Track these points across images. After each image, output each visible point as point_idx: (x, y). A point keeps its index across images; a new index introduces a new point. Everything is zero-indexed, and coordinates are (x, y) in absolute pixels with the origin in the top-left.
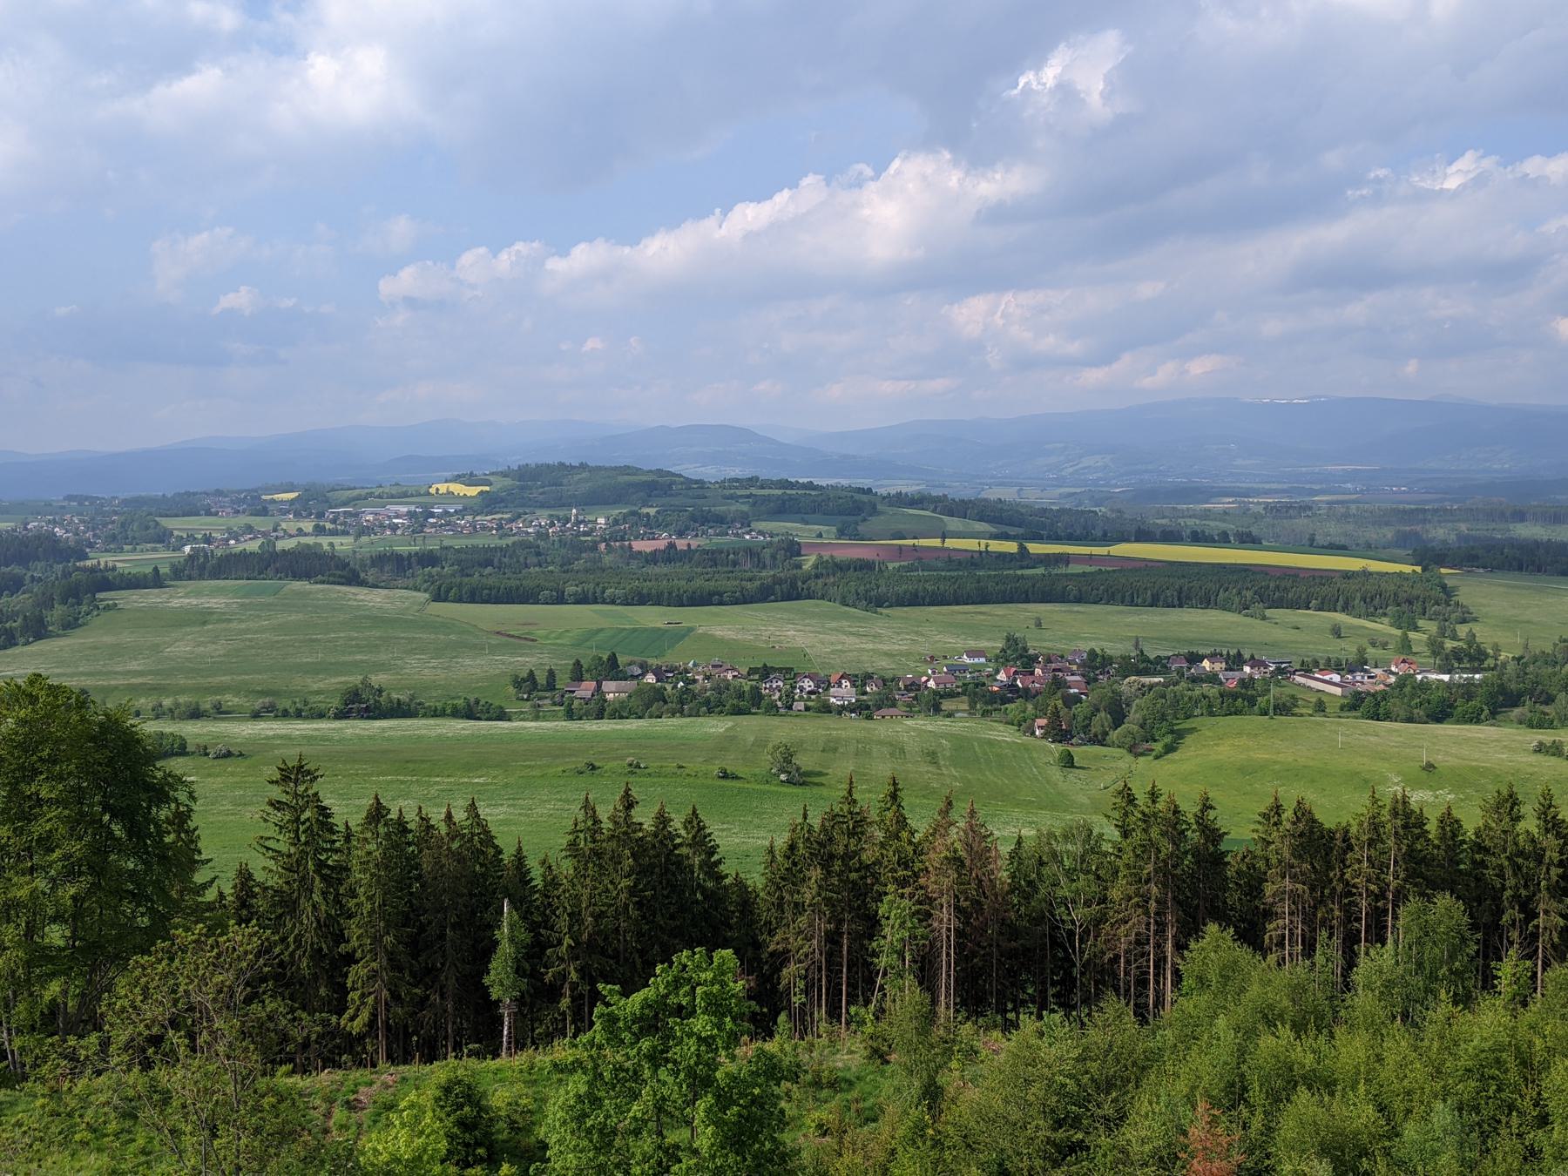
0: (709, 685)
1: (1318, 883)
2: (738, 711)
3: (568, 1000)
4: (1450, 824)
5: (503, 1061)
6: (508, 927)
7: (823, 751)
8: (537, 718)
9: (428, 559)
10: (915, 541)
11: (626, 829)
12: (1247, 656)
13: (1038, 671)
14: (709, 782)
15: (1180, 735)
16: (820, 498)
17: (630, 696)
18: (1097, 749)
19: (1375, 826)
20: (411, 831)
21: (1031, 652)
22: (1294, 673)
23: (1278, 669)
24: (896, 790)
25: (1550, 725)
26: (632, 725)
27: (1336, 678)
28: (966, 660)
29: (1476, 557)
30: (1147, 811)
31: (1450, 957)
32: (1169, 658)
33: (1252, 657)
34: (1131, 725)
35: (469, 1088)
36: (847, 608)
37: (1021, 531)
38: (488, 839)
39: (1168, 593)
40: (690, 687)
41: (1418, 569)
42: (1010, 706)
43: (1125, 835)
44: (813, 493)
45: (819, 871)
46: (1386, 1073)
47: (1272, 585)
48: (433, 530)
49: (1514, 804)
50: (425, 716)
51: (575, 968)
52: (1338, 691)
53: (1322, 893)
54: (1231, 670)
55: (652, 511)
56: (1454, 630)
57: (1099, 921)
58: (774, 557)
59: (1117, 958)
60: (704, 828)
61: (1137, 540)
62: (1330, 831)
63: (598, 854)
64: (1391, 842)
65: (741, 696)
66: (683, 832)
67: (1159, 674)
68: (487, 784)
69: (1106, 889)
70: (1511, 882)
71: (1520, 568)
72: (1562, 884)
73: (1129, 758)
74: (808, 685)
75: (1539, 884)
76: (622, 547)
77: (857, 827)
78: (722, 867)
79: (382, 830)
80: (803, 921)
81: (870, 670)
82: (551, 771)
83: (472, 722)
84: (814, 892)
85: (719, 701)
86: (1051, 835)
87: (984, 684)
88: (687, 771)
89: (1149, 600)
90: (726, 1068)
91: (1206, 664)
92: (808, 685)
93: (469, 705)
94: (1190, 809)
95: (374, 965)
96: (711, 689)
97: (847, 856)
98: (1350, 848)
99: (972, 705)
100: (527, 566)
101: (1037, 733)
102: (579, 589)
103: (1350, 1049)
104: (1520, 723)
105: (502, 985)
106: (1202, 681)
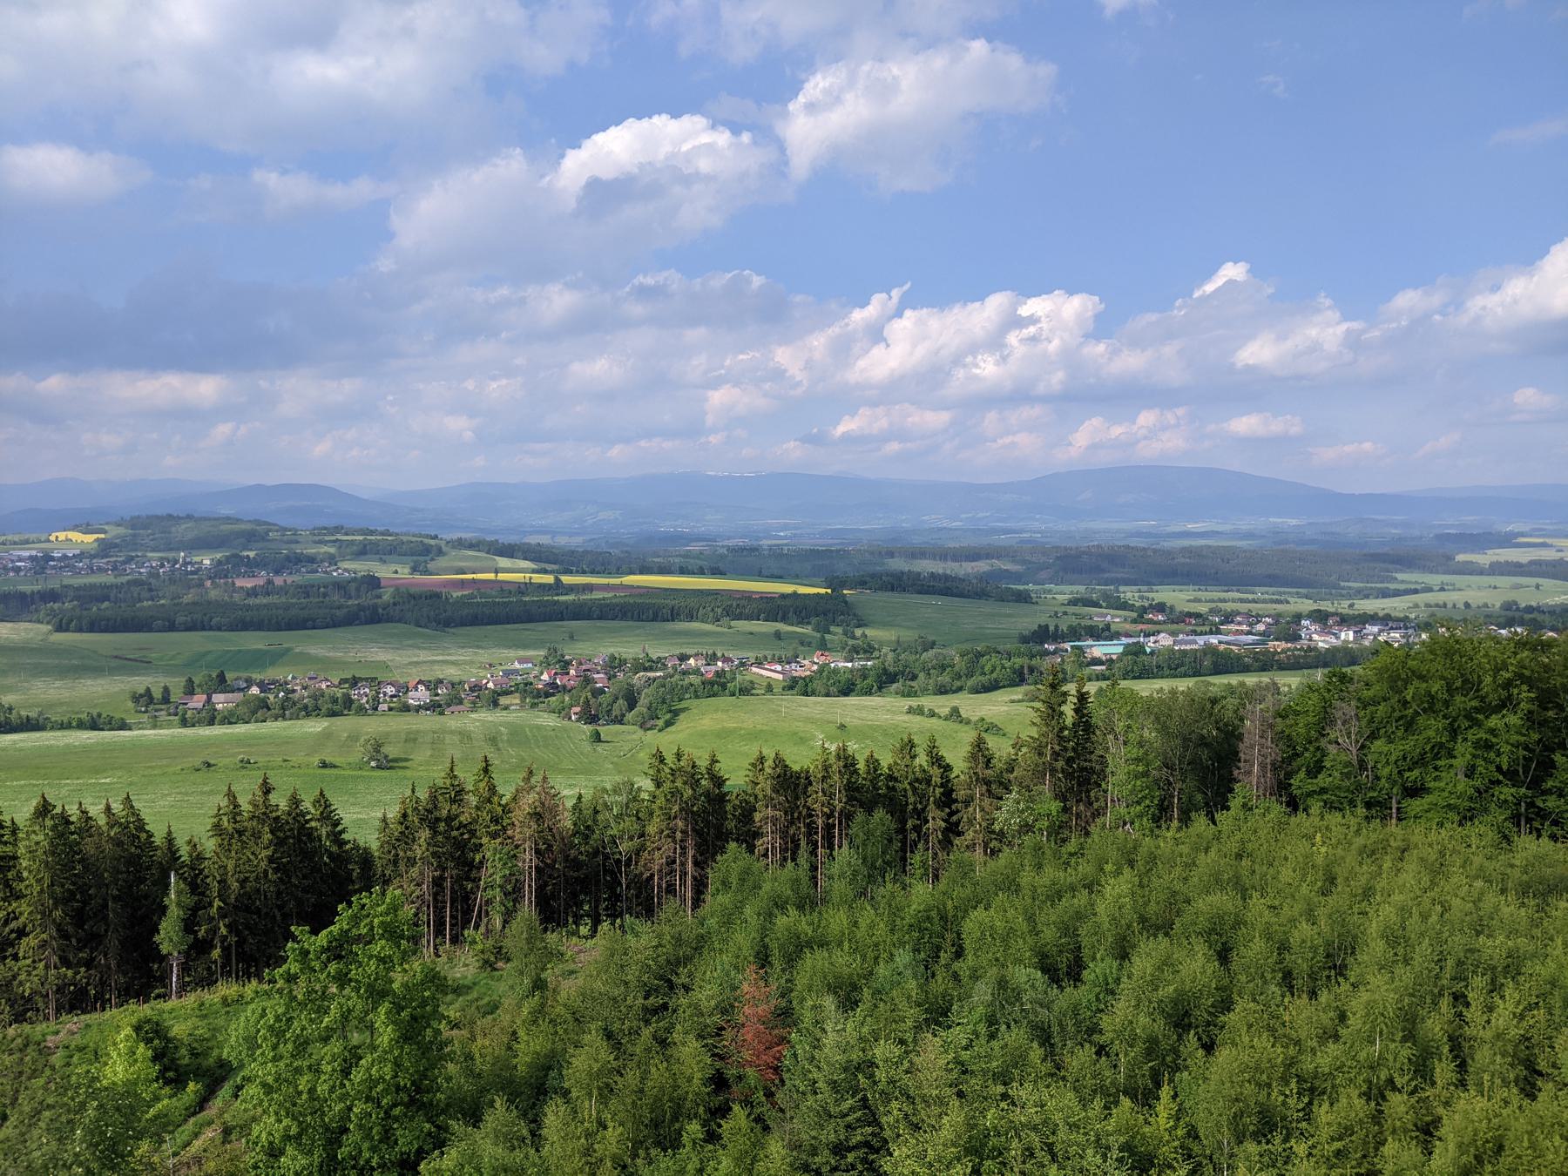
0: (306, 694)
1: (791, 811)
2: (333, 714)
3: (219, 950)
4: (873, 763)
5: (173, 1003)
6: (175, 894)
7: (406, 741)
8: (154, 727)
9: (52, 596)
10: (474, 576)
11: (265, 814)
12: (719, 655)
13: (572, 672)
14: (311, 771)
15: (676, 713)
16: (395, 543)
17: (237, 705)
18: (618, 727)
19: (826, 768)
20: (73, 823)
21: (567, 657)
22: (751, 665)
23: (741, 663)
24: (487, 765)
25: (916, 695)
26: (240, 729)
27: (779, 668)
28: (517, 665)
29: (865, 583)
30: (673, 767)
31: (883, 853)
32: (666, 658)
33: (723, 655)
34: (641, 708)
35: (157, 1025)
36: (420, 629)
37: (555, 567)
38: (141, 825)
39: (664, 611)
40: (290, 696)
41: (829, 591)
42: (552, 699)
43: (658, 785)
44: (390, 538)
45: (428, 832)
46: (861, 933)
47: (735, 604)
48: (54, 571)
49: (912, 747)
50: (52, 729)
51: (224, 925)
52: (780, 677)
53: (792, 816)
54: (709, 665)
55: (252, 554)
56: (853, 632)
57: (642, 848)
58: (358, 590)
59: (652, 875)
60: (330, 805)
61: (641, 573)
62: (796, 772)
63: (240, 833)
64: (836, 777)
65: (335, 701)
66: (313, 811)
67: (660, 669)
68: (114, 783)
69: (644, 826)
70: (911, 800)
71: (893, 590)
72: (943, 799)
73: (640, 732)
74: (390, 690)
75: (929, 800)
76: (225, 584)
77: (458, 795)
78: (343, 836)
79: (49, 823)
80: (414, 872)
81: (441, 677)
82: (171, 770)
83: (96, 733)
84: (424, 848)
85: (316, 706)
86: (605, 790)
87: (531, 684)
88: (291, 764)
89: (651, 616)
90: (398, 980)
91: (692, 661)
92: (390, 690)
93: (93, 718)
94: (703, 764)
95: (44, 936)
96: (309, 697)
97: (450, 819)
98: (810, 784)
99: (523, 699)
100: (140, 600)
101: (573, 718)
102: (189, 619)
103: (837, 920)
104: (897, 694)
105: (171, 940)
106: (689, 674)
